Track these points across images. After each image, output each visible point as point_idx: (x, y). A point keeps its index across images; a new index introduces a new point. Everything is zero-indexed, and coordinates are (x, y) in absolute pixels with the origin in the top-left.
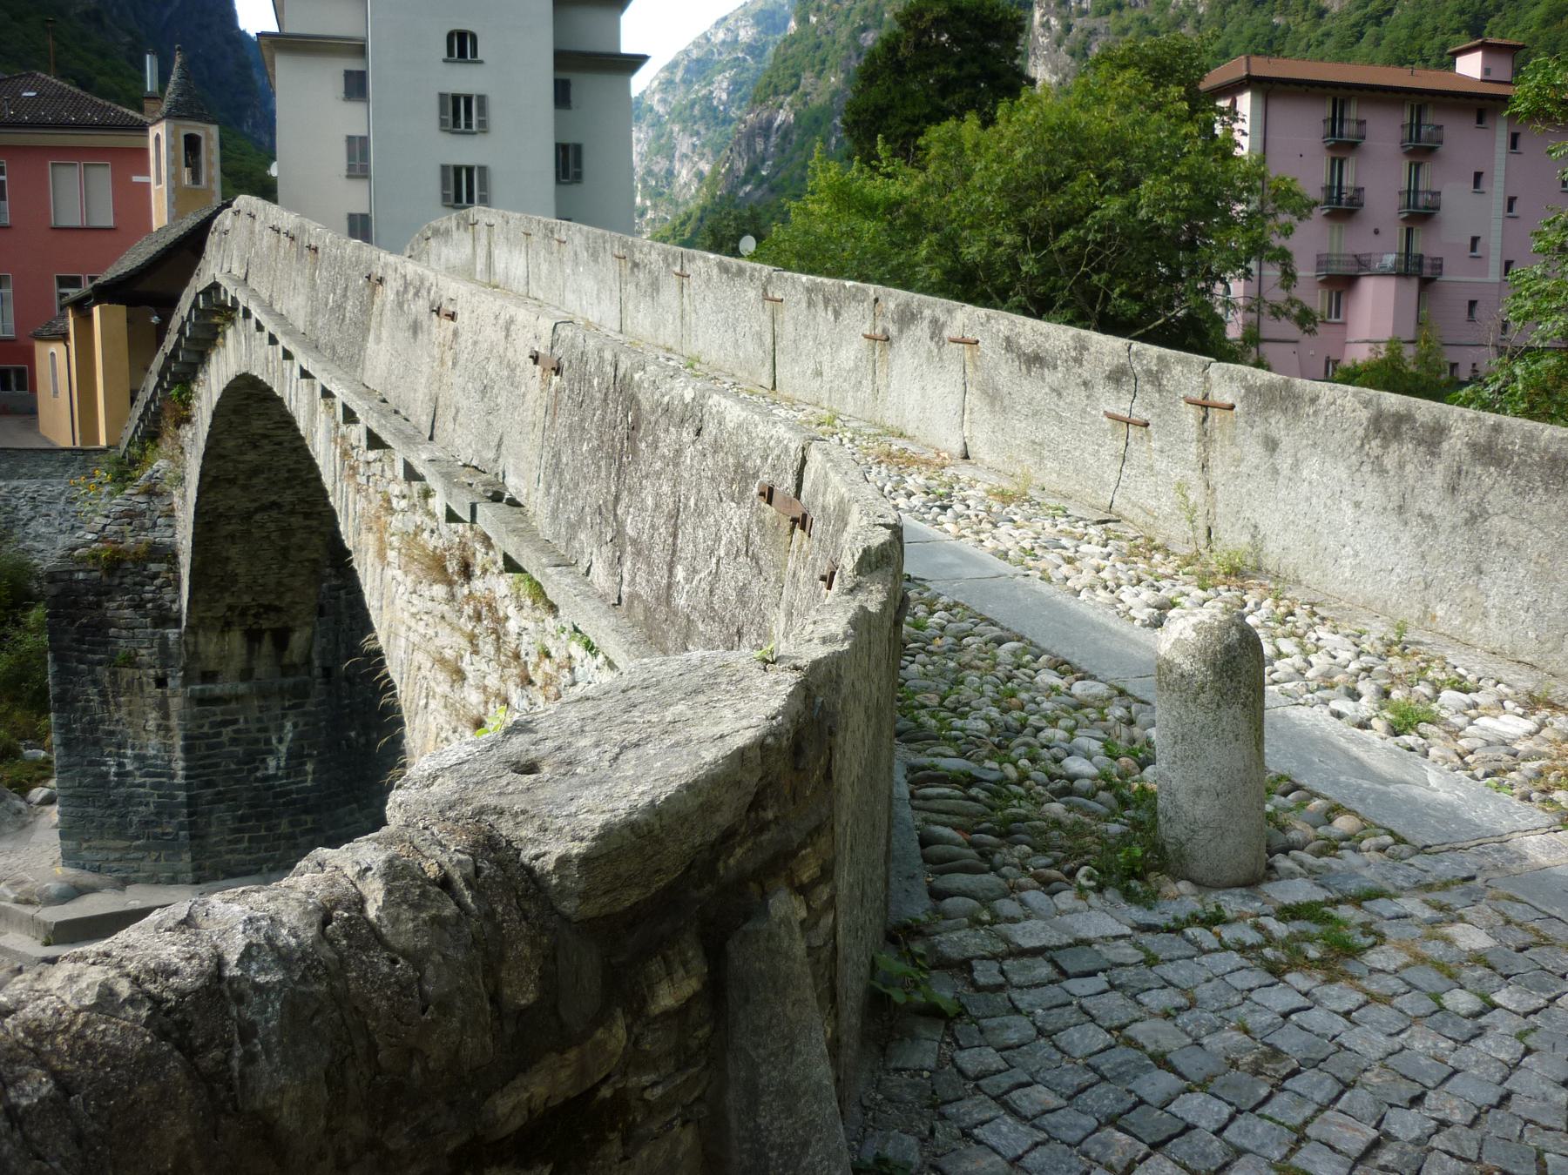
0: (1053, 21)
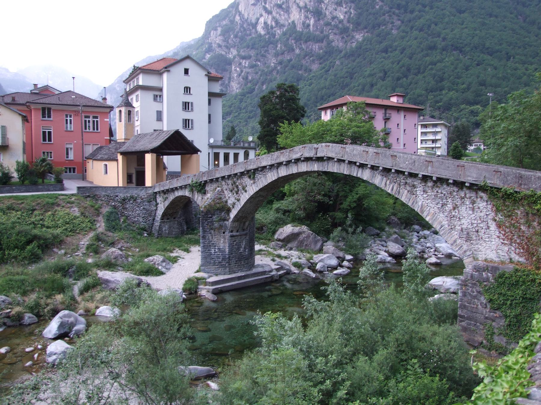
0: (238, 69)
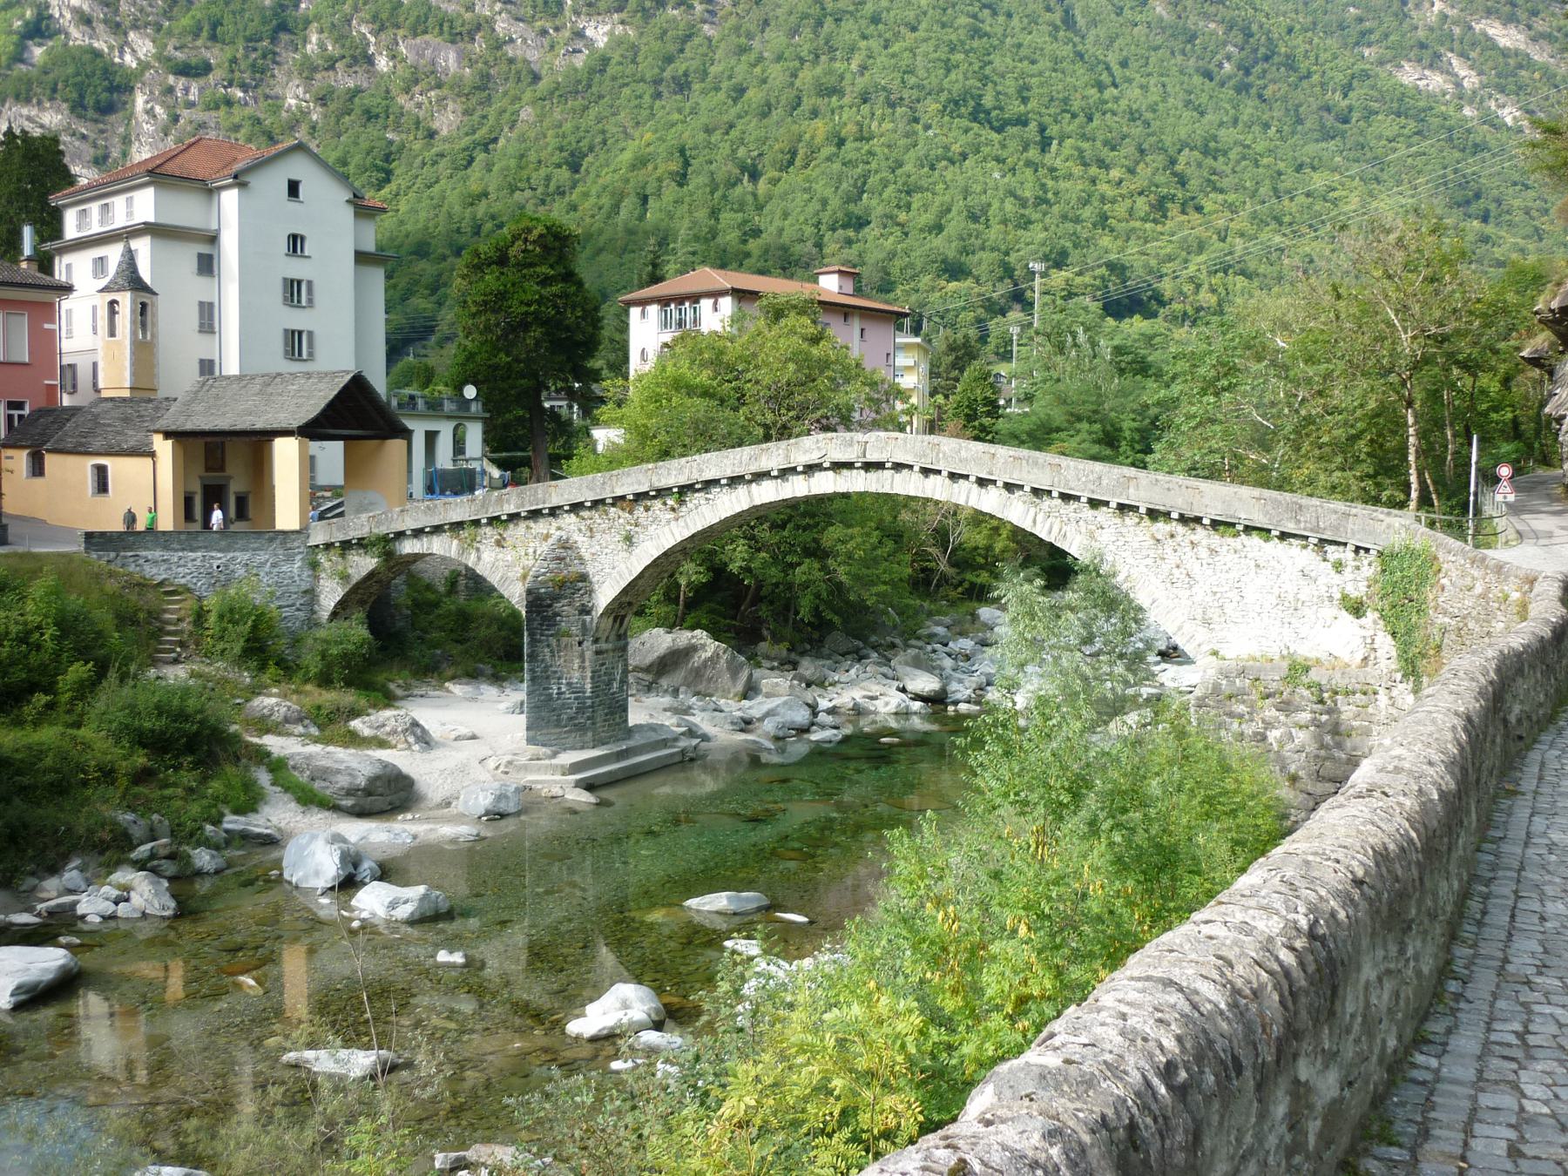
0: (158, 110)
